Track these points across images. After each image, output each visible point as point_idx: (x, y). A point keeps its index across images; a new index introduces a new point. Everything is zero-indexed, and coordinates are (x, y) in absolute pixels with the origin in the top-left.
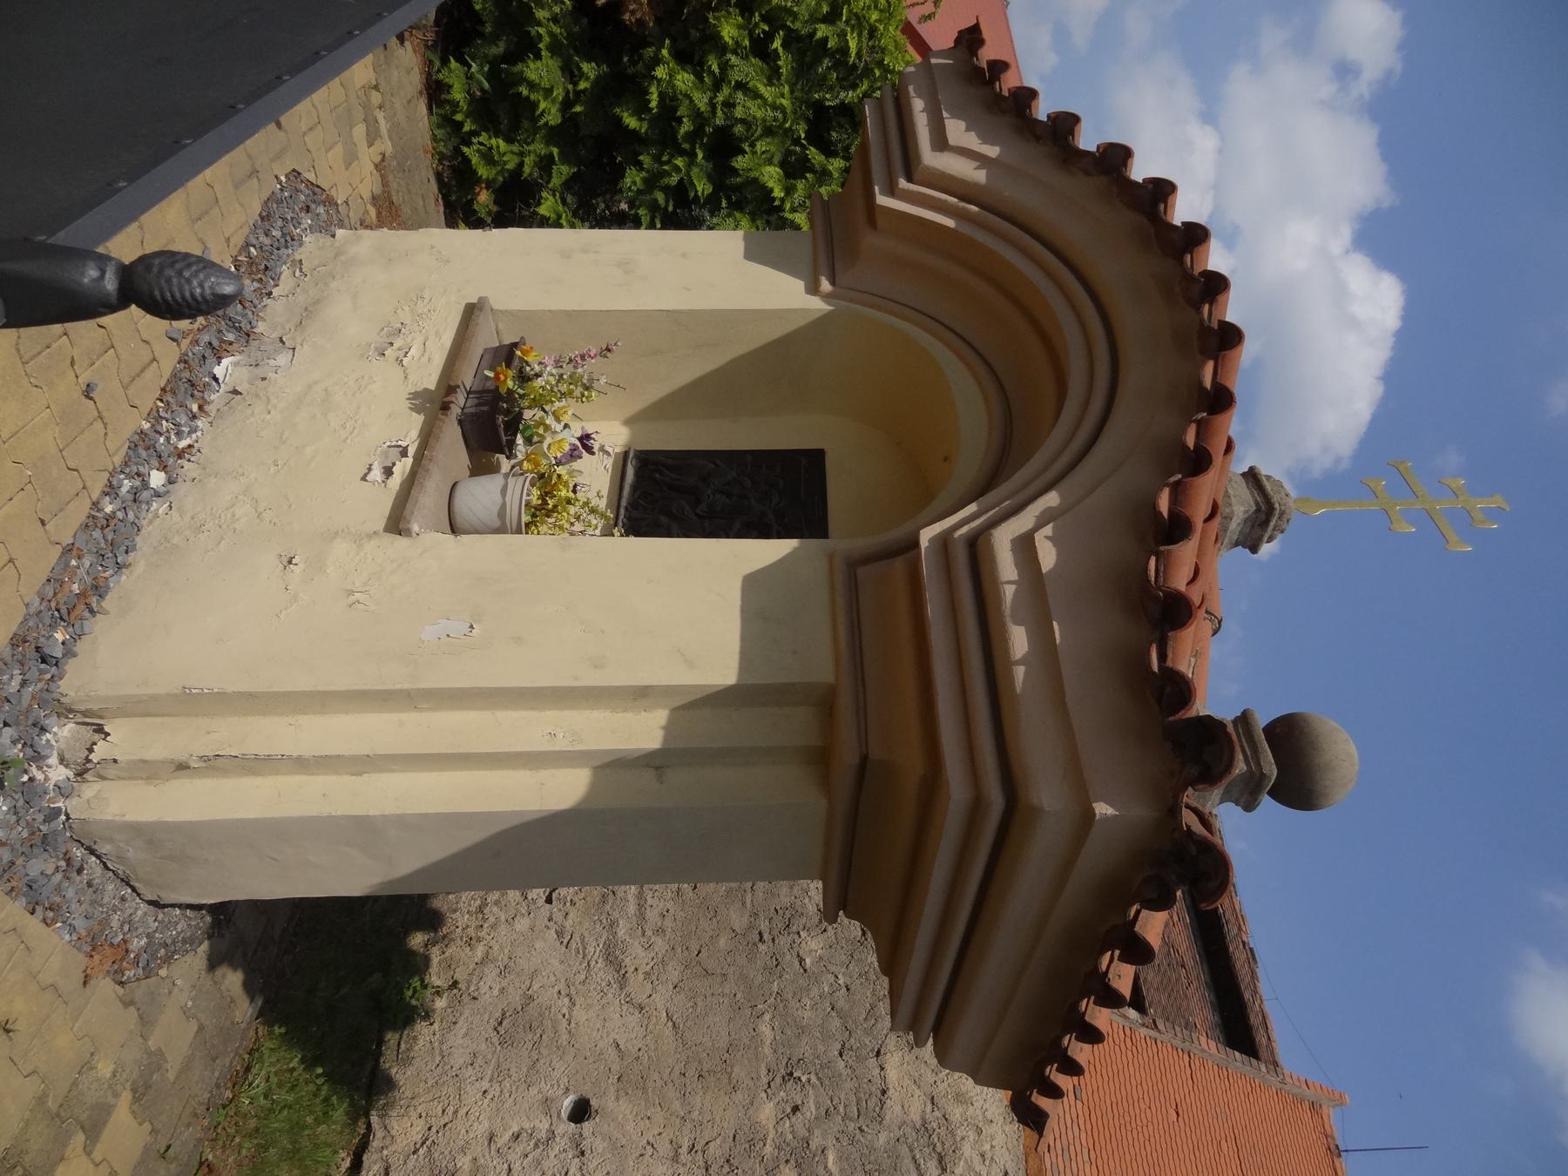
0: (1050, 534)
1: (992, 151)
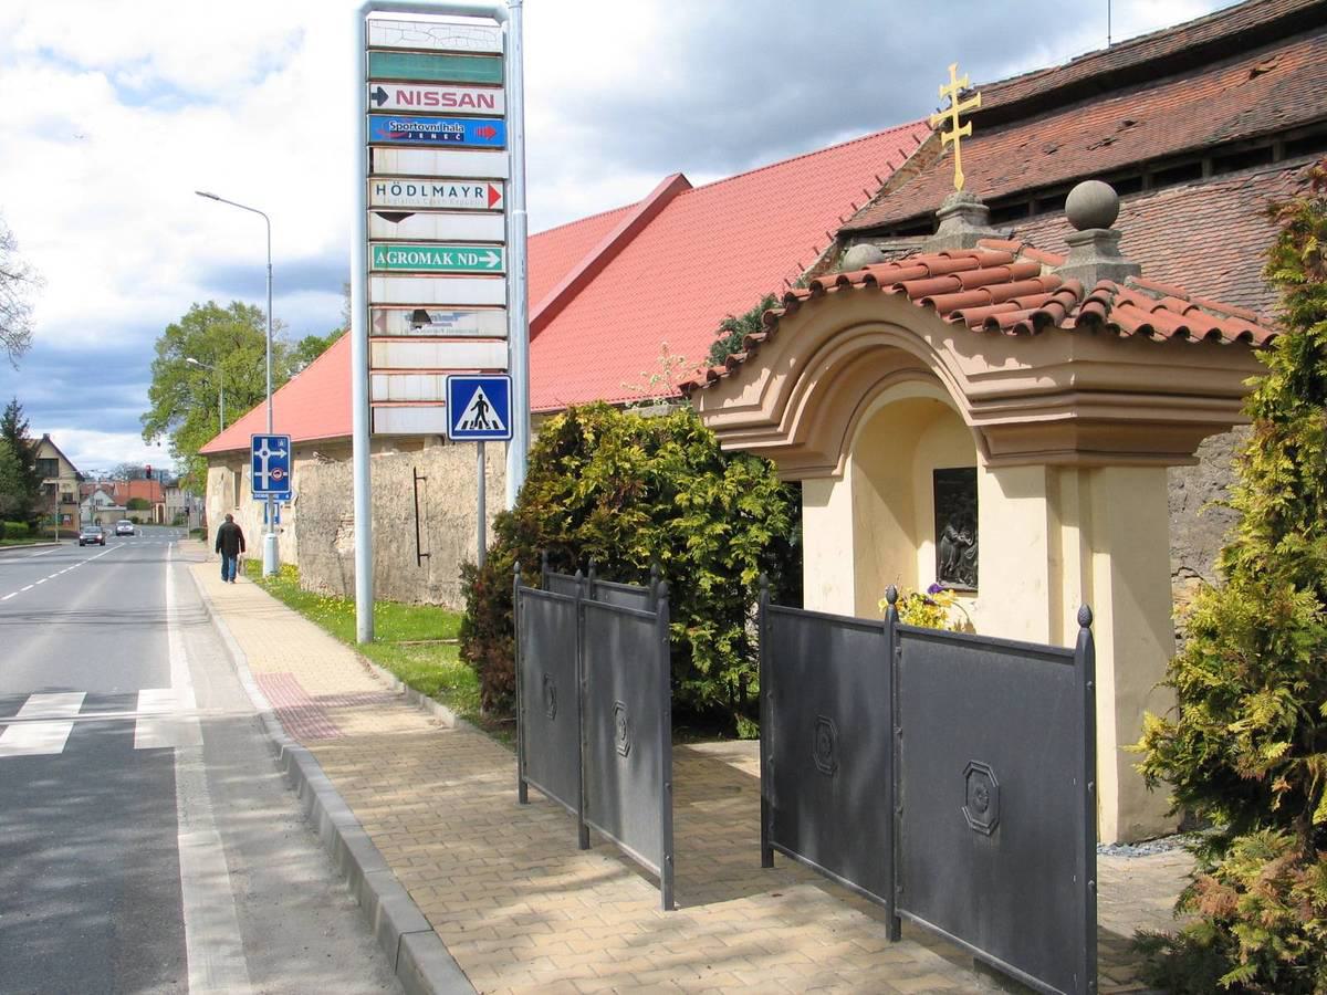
0: (872, 251)
1: (766, 372)
